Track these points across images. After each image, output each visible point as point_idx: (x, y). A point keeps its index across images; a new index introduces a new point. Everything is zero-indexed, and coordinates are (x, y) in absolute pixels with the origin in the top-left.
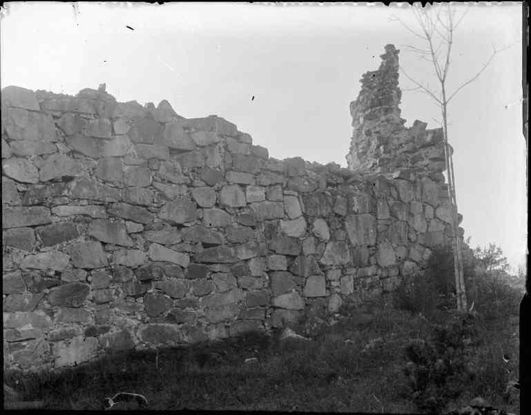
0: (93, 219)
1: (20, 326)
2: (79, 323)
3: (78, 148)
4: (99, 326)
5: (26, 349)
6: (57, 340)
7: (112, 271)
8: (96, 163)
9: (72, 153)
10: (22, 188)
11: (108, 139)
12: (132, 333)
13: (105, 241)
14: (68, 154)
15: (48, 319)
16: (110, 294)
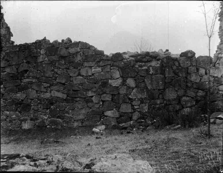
0: (33, 83)
1: (12, 116)
2: (28, 116)
3: (29, 60)
4: (34, 118)
5: (14, 123)
6: (23, 121)
7: (39, 100)
8: (35, 64)
9: (28, 62)
10: (11, 75)
11: (39, 56)
12: (45, 121)
13: (37, 90)
14: (26, 63)
15: (20, 114)
16: (38, 108)
